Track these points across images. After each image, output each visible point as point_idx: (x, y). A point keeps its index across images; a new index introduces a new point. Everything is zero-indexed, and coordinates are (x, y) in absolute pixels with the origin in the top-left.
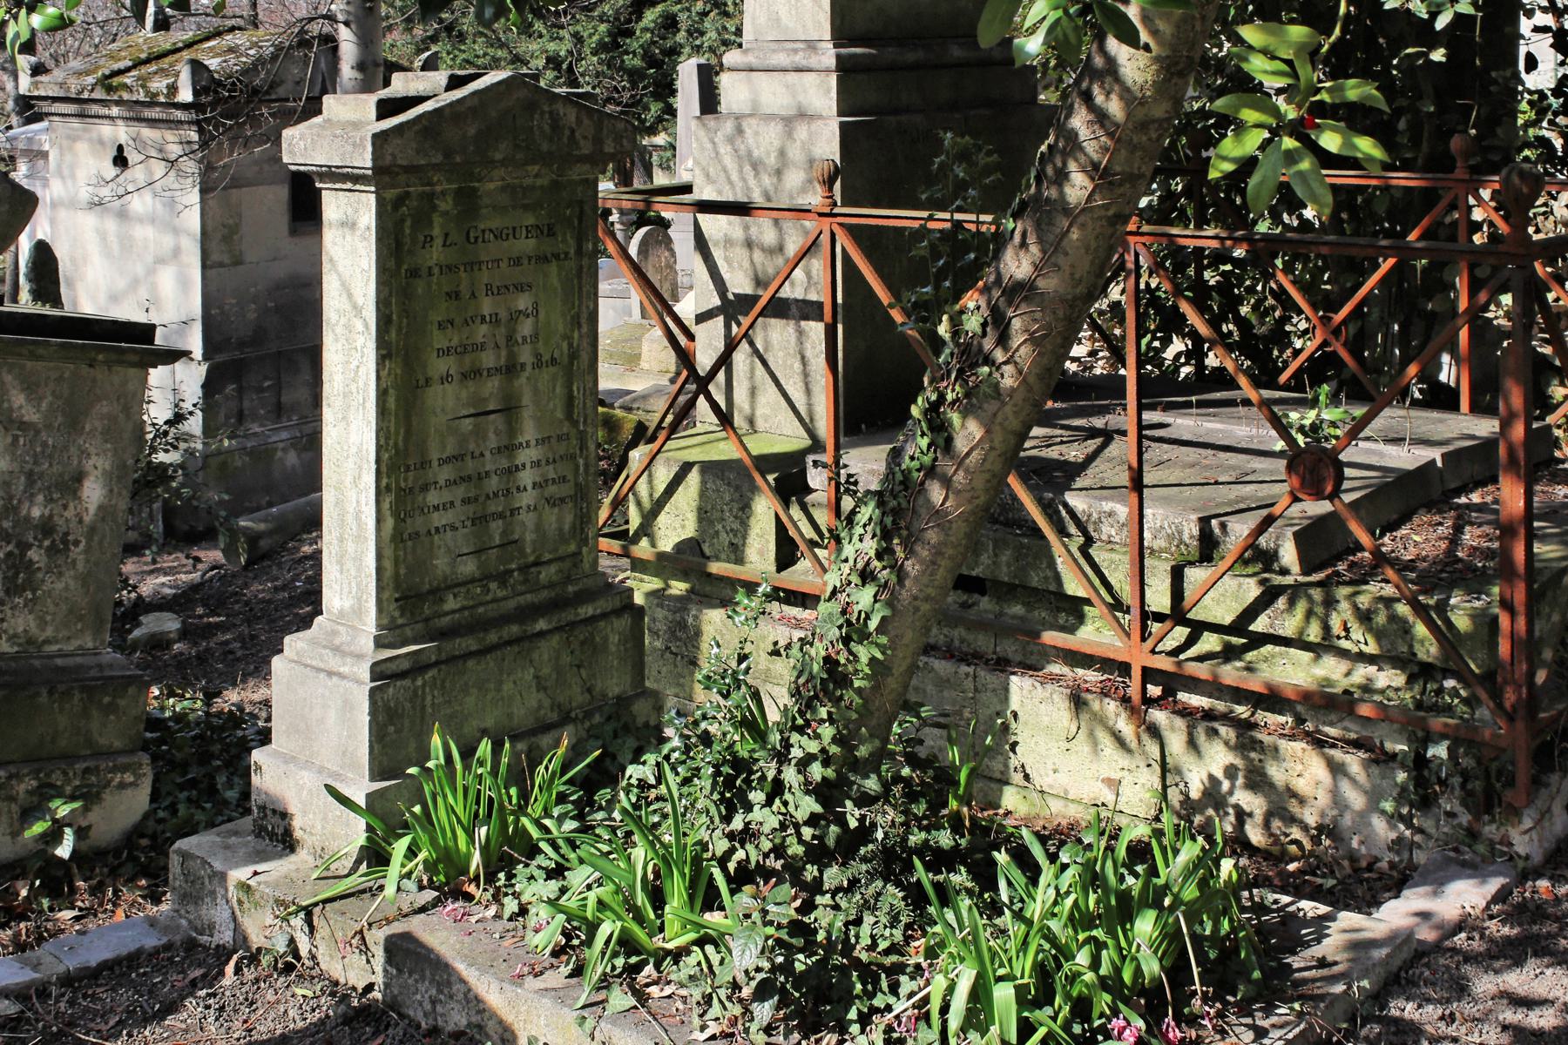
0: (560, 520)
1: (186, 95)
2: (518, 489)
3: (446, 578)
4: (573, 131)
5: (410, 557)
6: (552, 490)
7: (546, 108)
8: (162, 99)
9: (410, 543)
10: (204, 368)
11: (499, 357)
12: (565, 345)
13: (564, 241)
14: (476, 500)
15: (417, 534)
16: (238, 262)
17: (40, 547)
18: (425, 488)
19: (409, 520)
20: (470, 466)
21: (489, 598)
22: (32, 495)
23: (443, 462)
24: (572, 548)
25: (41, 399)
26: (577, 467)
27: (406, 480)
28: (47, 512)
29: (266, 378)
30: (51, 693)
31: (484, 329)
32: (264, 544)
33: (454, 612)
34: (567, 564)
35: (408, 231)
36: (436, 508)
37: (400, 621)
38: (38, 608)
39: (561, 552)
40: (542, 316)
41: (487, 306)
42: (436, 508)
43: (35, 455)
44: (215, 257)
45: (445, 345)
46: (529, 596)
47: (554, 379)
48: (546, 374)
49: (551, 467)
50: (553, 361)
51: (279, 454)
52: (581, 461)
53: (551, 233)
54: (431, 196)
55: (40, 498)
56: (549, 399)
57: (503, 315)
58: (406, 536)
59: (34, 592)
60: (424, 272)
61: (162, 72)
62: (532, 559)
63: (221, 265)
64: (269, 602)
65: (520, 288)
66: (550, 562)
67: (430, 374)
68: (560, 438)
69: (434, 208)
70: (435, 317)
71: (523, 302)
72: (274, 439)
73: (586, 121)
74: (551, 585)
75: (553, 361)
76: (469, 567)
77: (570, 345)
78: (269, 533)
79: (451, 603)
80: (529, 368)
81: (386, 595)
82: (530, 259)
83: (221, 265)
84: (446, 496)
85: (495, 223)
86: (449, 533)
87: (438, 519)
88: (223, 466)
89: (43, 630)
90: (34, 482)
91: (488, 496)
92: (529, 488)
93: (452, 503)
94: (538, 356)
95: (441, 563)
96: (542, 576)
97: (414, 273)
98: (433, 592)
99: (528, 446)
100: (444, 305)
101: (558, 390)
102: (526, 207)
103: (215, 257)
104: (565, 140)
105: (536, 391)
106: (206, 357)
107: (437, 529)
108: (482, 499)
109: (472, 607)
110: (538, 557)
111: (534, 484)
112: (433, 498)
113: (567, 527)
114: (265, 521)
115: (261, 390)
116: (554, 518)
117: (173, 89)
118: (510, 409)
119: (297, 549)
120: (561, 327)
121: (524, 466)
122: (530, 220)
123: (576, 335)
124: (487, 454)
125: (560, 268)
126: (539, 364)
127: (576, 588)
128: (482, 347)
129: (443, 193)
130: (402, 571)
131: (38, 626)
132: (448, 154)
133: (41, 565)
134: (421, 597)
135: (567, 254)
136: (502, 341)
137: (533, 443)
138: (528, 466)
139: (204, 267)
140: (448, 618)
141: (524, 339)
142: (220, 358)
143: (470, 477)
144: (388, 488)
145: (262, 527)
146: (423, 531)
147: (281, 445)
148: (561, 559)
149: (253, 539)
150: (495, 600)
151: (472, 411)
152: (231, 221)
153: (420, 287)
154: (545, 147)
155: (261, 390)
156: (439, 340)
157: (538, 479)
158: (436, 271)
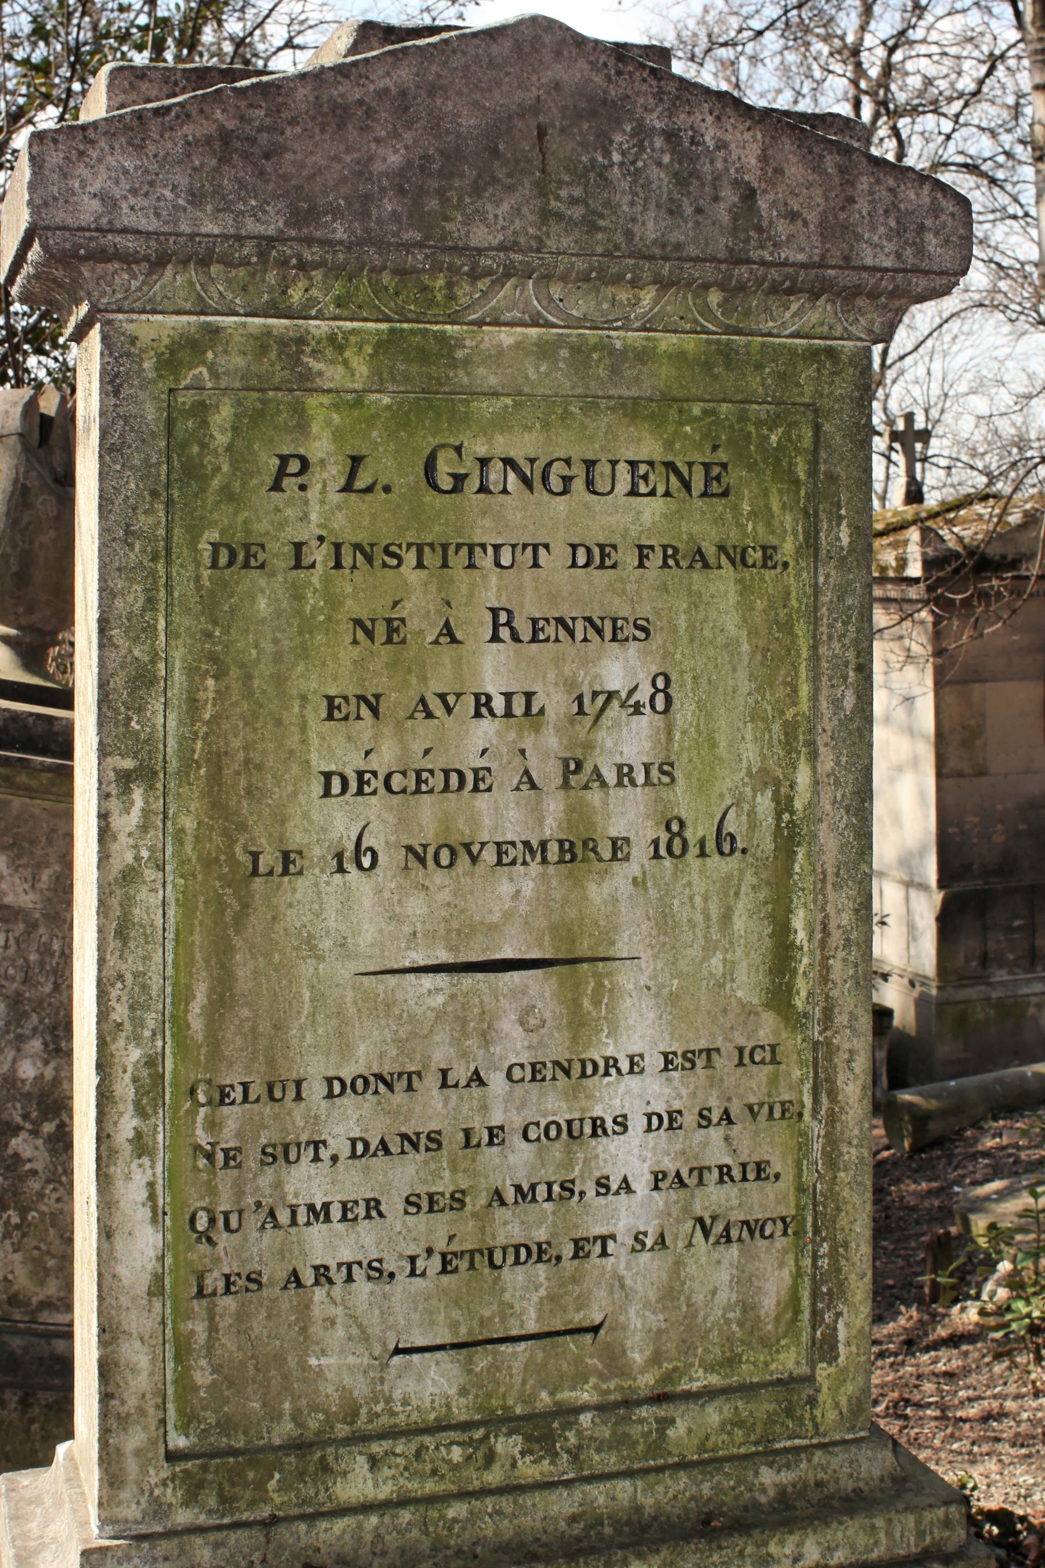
0: (744, 1280)
1: (915, 570)
2: (603, 1185)
3: (351, 1414)
4: (749, 195)
5: (228, 1341)
6: (715, 1198)
7: (655, 121)
8: (891, 574)
9: (228, 1303)
10: (938, 897)
11: (537, 815)
12: (765, 803)
13: (762, 514)
14: (458, 1200)
15: (254, 1278)
16: (981, 772)
17: (35, 1133)
18: (281, 1154)
19: (223, 1239)
20: (433, 1109)
21: (494, 1477)
22: (20, 1038)
23: (337, 1088)
24: (790, 1360)
25: (40, 865)
26: (803, 1148)
27: (212, 1125)
28: (49, 1072)
29: (1017, 917)
30: (25, 1403)
31: (486, 730)
32: (934, 1127)
33: (366, 1508)
34: (764, 1407)
35: (222, 439)
36: (320, 1213)
37: (183, 1517)
38: (30, 1242)
39: (747, 1373)
40: (685, 712)
41: (494, 669)
42: (320, 1213)
43: (27, 967)
44: (953, 764)
45: (351, 762)
46: (624, 1488)
47: (729, 888)
48: (704, 875)
49: (716, 1134)
50: (724, 842)
51: (1032, 1010)
52: (817, 1129)
53: (717, 488)
54: (293, 348)
55: (36, 1045)
56: (710, 948)
57: (555, 702)
58: (214, 1281)
59: (23, 1211)
60: (279, 552)
61: (894, 545)
62: (646, 1381)
63: (960, 775)
64: (913, 1209)
65: (611, 630)
66: (708, 1394)
67: (296, 838)
68: (743, 1057)
69: (306, 382)
70: (316, 683)
71: (619, 669)
72: (1025, 991)
73: (795, 171)
74: (708, 1463)
75: (724, 842)
76: (432, 1385)
77: (783, 805)
78: (943, 1113)
79: (358, 1482)
80: (640, 852)
81: (134, 1439)
82: (643, 552)
83: (960, 775)
84: (353, 1183)
85: (522, 445)
86: (362, 1287)
87: (325, 1245)
88: (962, 1018)
89: (41, 1283)
90: (25, 1015)
91: (498, 1195)
92: (641, 1184)
93: (373, 1206)
94: (674, 828)
95: (338, 1366)
96: (677, 1432)
97: (242, 555)
98: (299, 1446)
99: (635, 1065)
100: (348, 654)
101: (739, 923)
102: (632, 410)
103: (953, 764)
104: (722, 214)
105: (665, 922)
106: (941, 885)
107: (322, 1274)
108: (476, 1203)
109: (431, 1500)
110: (668, 1378)
111: (658, 1179)
112: (307, 1183)
113: (769, 1303)
114: (938, 1097)
115: (1010, 929)
116: (724, 1276)
117: (902, 563)
118: (572, 962)
119: (976, 1140)
120: (750, 753)
121: (622, 1123)
122: (648, 447)
123: (803, 777)
124: (497, 1081)
125: (745, 589)
126: (673, 841)
127: (786, 1477)
128: (480, 781)
129: (336, 343)
130: (203, 1377)
131: (33, 1274)
132: (304, 215)
133: (39, 1166)
134: (260, 1458)
135: (768, 552)
136: (547, 772)
137: (654, 1061)
138: (637, 1124)
139: (940, 775)
140: (340, 1525)
141: (625, 773)
142: (957, 887)
143: (435, 1140)
144: (141, 1146)
145: (934, 1104)
146: (274, 1271)
147: (1034, 1000)
148: (747, 1390)
149: (920, 1118)
150: (513, 1489)
151: (444, 956)
152: (972, 722)
153: (264, 597)
154: (651, 228)
155: (1010, 929)
156: (339, 750)
157: (670, 1165)
158: (320, 555)
